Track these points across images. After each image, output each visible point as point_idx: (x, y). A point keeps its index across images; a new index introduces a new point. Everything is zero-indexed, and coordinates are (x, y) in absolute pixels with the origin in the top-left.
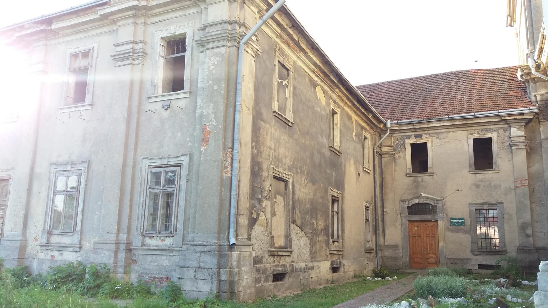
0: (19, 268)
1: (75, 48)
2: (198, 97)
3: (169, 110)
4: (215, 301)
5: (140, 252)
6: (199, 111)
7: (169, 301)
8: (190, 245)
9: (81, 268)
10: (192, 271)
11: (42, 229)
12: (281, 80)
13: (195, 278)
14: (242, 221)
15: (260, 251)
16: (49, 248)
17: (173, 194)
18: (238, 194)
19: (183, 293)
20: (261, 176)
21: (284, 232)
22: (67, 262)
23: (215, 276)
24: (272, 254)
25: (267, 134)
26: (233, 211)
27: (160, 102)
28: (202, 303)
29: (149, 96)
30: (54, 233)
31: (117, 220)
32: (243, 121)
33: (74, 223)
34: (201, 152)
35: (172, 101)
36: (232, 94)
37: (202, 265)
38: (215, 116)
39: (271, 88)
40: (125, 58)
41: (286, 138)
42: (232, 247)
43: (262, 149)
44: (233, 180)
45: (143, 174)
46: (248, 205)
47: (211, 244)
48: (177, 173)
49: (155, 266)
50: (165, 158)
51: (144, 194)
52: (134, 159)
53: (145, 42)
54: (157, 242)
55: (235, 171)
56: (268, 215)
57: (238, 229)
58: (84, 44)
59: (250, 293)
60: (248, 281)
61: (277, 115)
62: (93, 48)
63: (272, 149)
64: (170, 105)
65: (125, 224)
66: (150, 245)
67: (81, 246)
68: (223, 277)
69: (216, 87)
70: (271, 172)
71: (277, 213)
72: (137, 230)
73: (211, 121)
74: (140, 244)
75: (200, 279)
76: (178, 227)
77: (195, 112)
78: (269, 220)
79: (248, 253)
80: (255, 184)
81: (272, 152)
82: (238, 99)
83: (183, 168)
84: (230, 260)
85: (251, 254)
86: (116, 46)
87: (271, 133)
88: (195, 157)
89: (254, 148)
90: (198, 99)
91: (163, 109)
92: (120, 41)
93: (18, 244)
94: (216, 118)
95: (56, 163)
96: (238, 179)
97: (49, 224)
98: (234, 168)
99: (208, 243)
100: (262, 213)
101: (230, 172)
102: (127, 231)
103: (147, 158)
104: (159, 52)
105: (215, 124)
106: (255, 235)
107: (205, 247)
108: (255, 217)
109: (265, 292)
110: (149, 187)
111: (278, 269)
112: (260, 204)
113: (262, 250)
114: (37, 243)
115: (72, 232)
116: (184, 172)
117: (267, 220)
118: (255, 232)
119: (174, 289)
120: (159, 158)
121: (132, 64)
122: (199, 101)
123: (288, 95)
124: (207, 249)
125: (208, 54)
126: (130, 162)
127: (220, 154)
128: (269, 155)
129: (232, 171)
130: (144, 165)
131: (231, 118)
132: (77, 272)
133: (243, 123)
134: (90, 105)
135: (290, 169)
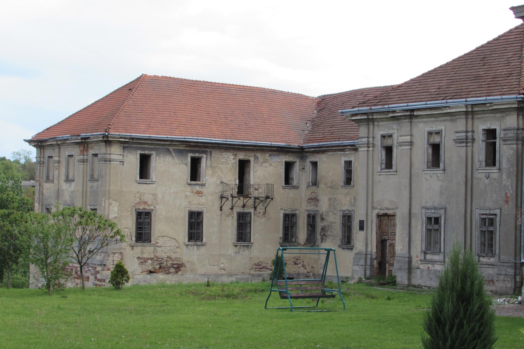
11: (420, 250)
23: (513, 279)
37: (507, 273)
38: (512, 187)
66: (483, 262)
69: (511, 169)
72: (475, 253)
73: (510, 190)
86: (456, 132)
116: (498, 219)
130: (477, 213)
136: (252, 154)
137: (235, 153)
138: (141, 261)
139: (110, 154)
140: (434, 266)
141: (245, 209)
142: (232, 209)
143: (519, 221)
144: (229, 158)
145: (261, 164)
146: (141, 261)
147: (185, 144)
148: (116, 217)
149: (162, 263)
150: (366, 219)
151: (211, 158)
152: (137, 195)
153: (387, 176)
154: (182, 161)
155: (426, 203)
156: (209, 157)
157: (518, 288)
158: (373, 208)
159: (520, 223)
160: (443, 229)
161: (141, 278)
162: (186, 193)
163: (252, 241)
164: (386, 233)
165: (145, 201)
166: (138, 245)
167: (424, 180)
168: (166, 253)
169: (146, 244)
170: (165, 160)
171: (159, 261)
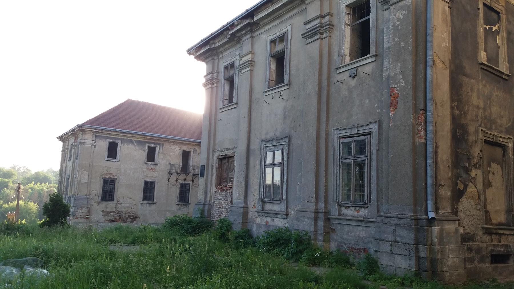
0: (242, 231)
1: (274, 35)
2: (385, 58)
3: (356, 79)
4: (414, 279)
5: (337, 222)
6: (385, 74)
7: (367, 274)
8: (385, 217)
9: (288, 233)
10: (387, 245)
11: (258, 198)
12: (489, 26)
13: (392, 253)
14: (444, 192)
15: (471, 228)
16: (264, 214)
17: (364, 164)
18: (436, 162)
19: (380, 267)
20: (467, 141)
21: (504, 207)
22: (277, 228)
23: (413, 253)
24: (488, 232)
25: (472, 90)
26: (430, 181)
27: (347, 72)
28: (399, 280)
29: (337, 67)
30: (267, 201)
31: (315, 190)
32: (437, 78)
33: (281, 192)
34: (390, 117)
35: (358, 68)
36: (421, 48)
37: (398, 238)
38: (403, 76)
39: (475, 36)
40: (314, 34)
41: (500, 94)
42: (431, 221)
43: (466, 109)
44: (428, 147)
45: (336, 145)
46: (450, 175)
47: (406, 217)
48: (367, 142)
49: (352, 236)
50: (354, 128)
51: (337, 164)
52: (326, 131)
53: (331, 14)
54: (352, 212)
55: (430, 136)
56: (480, 186)
57: (438, 201)
58: (280, 29)
59: (459, 275)
60: (455, 260)
61: (485, 68)
62: (288, 31)
63: (480, 108)
64: (357, 73)
65: (322, 194)
66: (346, 215)
67: (288, 214)
68: (423, 254)
69: (402, 44)
70: (481, 136)
71: (494, 184)
72: (333, 200)
73: (399, 82)
74: (337, 214)
75: (397, 254)
76: (371, 197)
77: (382, 75)
78: (482, 192)
79: (453, 230)
80: (460, 151)
81: (480, 112)
82: (429, 53)
83: (373, 136)
84: (429, 235)
85: (457, 231)
86: (306, 24)
87: (478, 90)
88: (384, 124)
89: (455, 108)
90: (384, 60)
91: (351, 78)
92: (309, 18)
93: (241, 210)
94: (404, 78)
95: (265, 140)
96: (435, 145)
97: (263, 193)
98: (428, 132)
99: (403, 216)
100: (471, 184)
101: (424, 137)
102: (325, 201)
103: (338, 129)
104: (345, 20)
105: (403, 85)
106: (464, 209)
107: (400, 220)
108: (462, 189)
109: (481, 275)
110: (342, 158)
111: (497, 249)
112: (468, 174)
113: (474, 227)
114: (255, 210)
115: (280, 201)
116: (374, 140)
117: (478, 192)
118: (463, 206)
119: (371, 262)
120: (349, 128)
121: (320, 38)
122: (386, 63)
123: (501, 42)
124: (402, 222)
125: (392, 9)
126: (323, 135)
127: (410, 117)
128: (477, 116)
129: (426, 135)
130: (335, 136)
131: (421, 76)
132: (285, 237)
133: (437, 80)
134: (287, 85)
135: (508, 131)
136: (193, 147)
137: (180, 146)
138: (105, 213)
139: (84, 140)
140: (273, 220)
141: (186, 181)
142: (176, 181)
143: (421, 137)
144: (176, 149)
145: (198, 154)
146: (105, 213)
147: (144, 137)
148: (86, 182)
149: (121, 215)
150: (207, 164)
151: (163, 148)
152: (105, 169)
153: (228, 111)
154: (141, 148)
155: (267, 133)
156: (161, 147)
157: (426, 271)
158: (214, 151)
159: (423, 140)
160: (286, 167)
161: (104, 225)
162: (143, 169)
163: (190, 202)
164: (225, 178)
165: (111, 173)
166: (103, 202)
167: (265, 104)
168: (125, 208)
169: (109, 202)
170: (128, 146)
171: (120, 214)
